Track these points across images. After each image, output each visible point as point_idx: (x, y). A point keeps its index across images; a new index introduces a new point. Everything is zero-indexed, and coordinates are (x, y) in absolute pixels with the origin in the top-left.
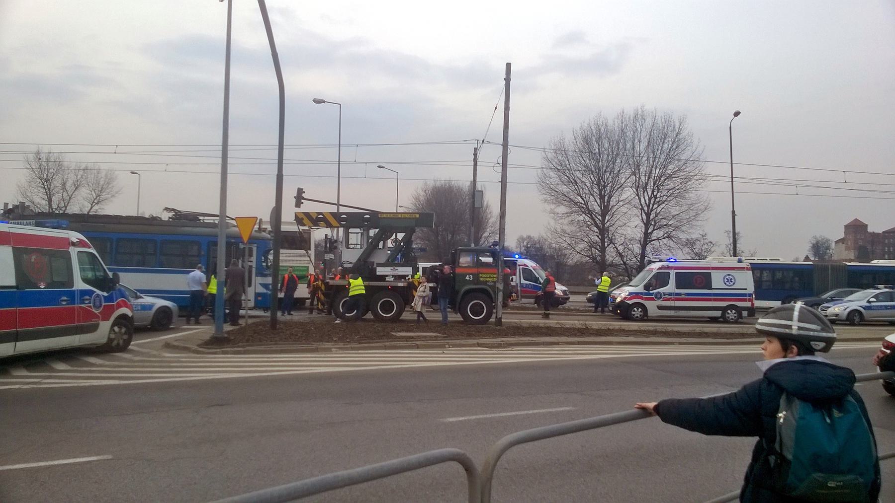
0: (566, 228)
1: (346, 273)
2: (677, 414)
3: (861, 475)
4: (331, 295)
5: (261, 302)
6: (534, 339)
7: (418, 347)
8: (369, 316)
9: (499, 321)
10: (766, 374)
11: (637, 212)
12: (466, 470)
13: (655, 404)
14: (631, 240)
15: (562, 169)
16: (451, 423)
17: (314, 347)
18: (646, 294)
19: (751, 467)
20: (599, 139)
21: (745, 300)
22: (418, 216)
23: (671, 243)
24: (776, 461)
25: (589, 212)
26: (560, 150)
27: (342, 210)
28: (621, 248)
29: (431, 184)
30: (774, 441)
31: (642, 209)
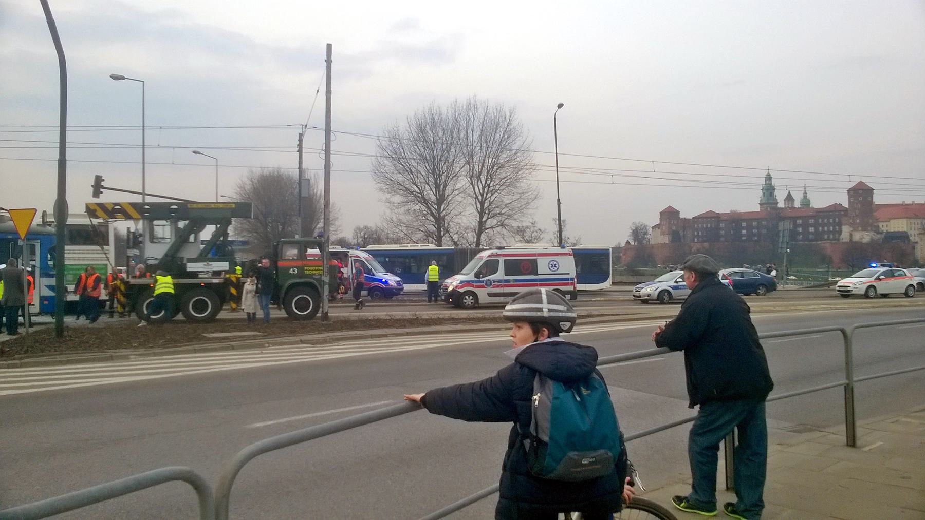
0: (402, 217)
1: (152, 270)
2: (448, 404)
3: (610, 449)
4: (135, 295)
5: (47, 306)
6: (362, 332)
7: (233, 348)
8: (180, 317)
9: (325, 316)
10: (517, 359)
11: (471, 200)
12: (196, 488)
13: (423, 395)
14: (466, 229)
15: (397, 158)
16: (258, 428)
17: (108, 354)
18: (477, 282)
19: (508, 454)
20: (433, 127)
21: (568, 284)
22: (234, 206)
23: (504, 231)
24: (532, 444)
25: (425, 201)
26: (394, 138)
27: (149, 199)
28: (456, 237)
29: (257, 172)
30: (529, 425)
31: (477, 198)
